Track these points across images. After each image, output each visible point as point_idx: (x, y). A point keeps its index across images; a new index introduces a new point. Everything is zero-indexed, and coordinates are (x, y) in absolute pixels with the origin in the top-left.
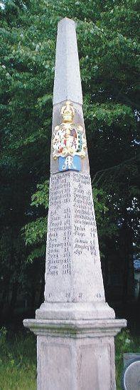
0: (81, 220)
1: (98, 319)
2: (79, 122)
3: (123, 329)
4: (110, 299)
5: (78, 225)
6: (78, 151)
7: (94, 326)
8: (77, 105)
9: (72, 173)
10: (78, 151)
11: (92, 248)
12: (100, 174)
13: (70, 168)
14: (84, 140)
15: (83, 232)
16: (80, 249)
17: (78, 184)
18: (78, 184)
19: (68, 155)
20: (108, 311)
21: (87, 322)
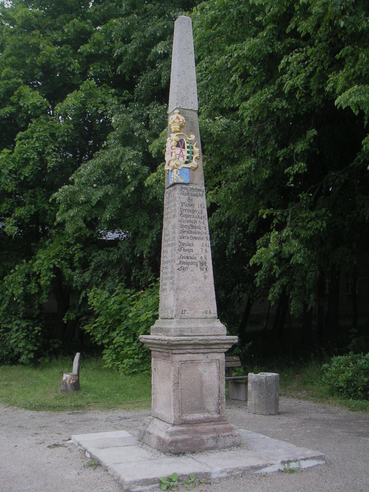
0: (189, 235)
1: (159, 351)
2: (191, 131)
3: (234, 346)
4: (225, 311)
5: (184, 241)
6: (186, 163)
7: (192, 342)
8: (190, 112)
9: (178, 187)
10: (186, 163)
11: (203, 264)
12: (182, 432)
13: (175, 181)
14: (197, 150)
15: (191, 248)
16: (185, 266)
17: (187, 197)
18: (187, 197)
19: (174, 168)
20: (220, 326)
21: (197, 351)
